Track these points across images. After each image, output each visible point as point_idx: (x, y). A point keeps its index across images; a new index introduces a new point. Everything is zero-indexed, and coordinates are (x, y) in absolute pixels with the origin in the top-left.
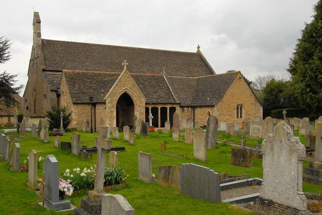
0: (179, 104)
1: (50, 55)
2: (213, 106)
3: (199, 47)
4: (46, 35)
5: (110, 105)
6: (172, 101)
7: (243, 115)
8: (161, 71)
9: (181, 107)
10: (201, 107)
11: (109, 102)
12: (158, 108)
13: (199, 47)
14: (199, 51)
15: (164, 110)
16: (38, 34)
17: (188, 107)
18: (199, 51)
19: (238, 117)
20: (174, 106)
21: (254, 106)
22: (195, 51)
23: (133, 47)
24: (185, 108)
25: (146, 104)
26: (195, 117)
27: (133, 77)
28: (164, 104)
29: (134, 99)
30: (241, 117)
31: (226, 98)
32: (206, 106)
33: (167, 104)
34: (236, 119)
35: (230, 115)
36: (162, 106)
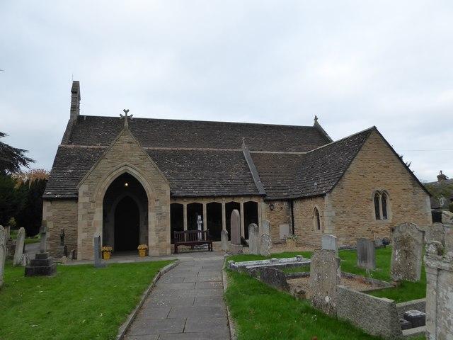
0: (263, 196)
1: (86, 132)
2: (323, 196)
3: (316, 119)
4: (84, 111)
5: (87, 199)
6: (251, 191)
7: (390, 213)
8: (239, 146)
9: (267, 201)
10: (302, 199)
11: (85, 194)
12: (202, 205)
13: (316, 119)
14: (316, 124)
15: (214, 211)
16: (75, 108)
17: (282, 200)
18: (316, 124)
19: (378, 217)
20: (254, 200)
21: (411, 195)
22: (312, 124)
23: (248, 122)
24: (276, 204)
25: (173, 197)
26: (295, 219)
27: (152, 155)
28: (233, 197)
29: (146, 185)
30: (385, 214)
31: (349, 179)
32: (310, 198)
33: (239, 196)
34: (375, 221)
35: (361, 214)
36: (247, 200)
